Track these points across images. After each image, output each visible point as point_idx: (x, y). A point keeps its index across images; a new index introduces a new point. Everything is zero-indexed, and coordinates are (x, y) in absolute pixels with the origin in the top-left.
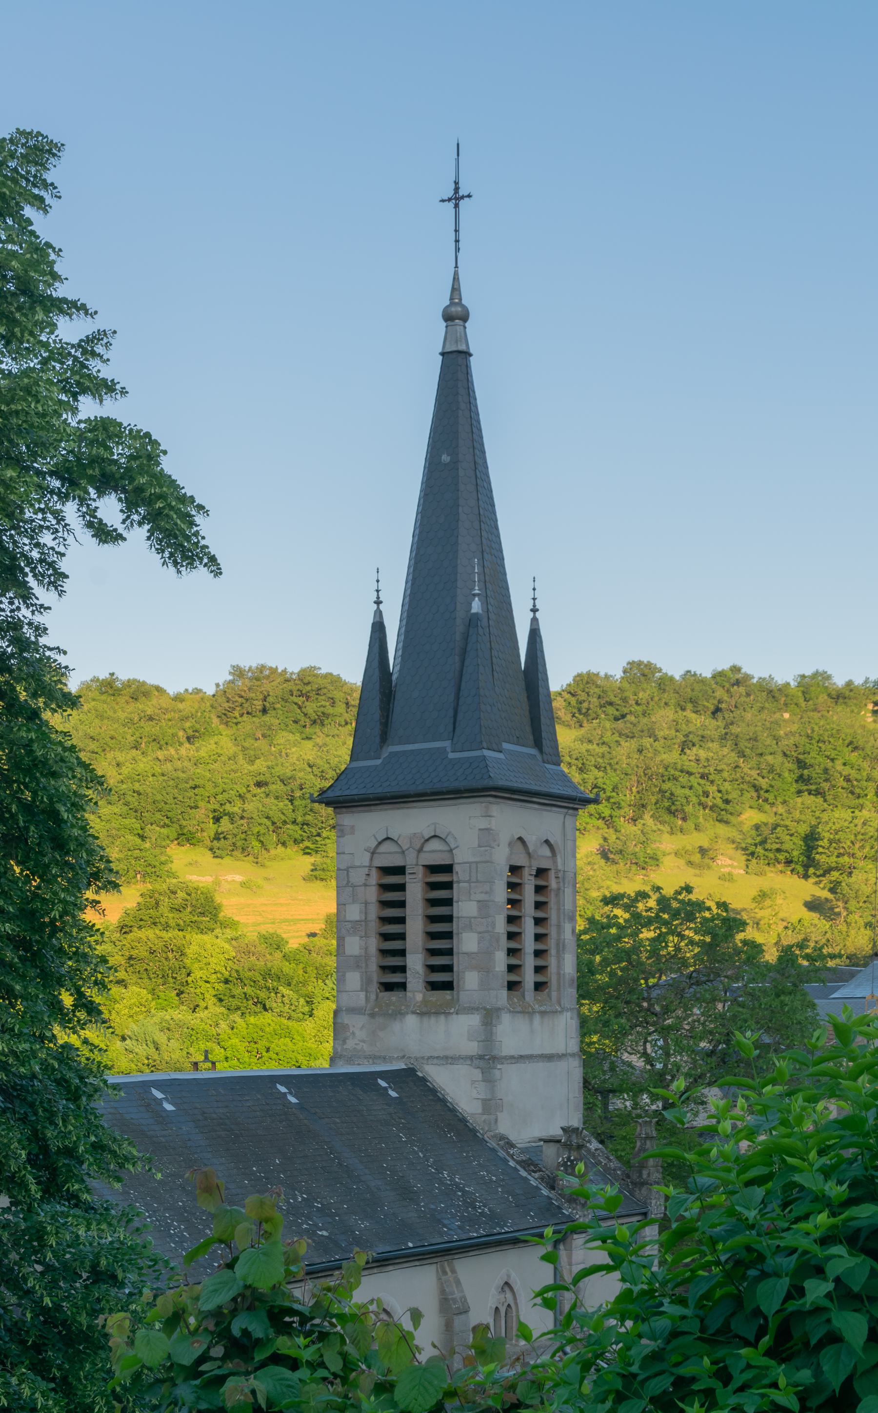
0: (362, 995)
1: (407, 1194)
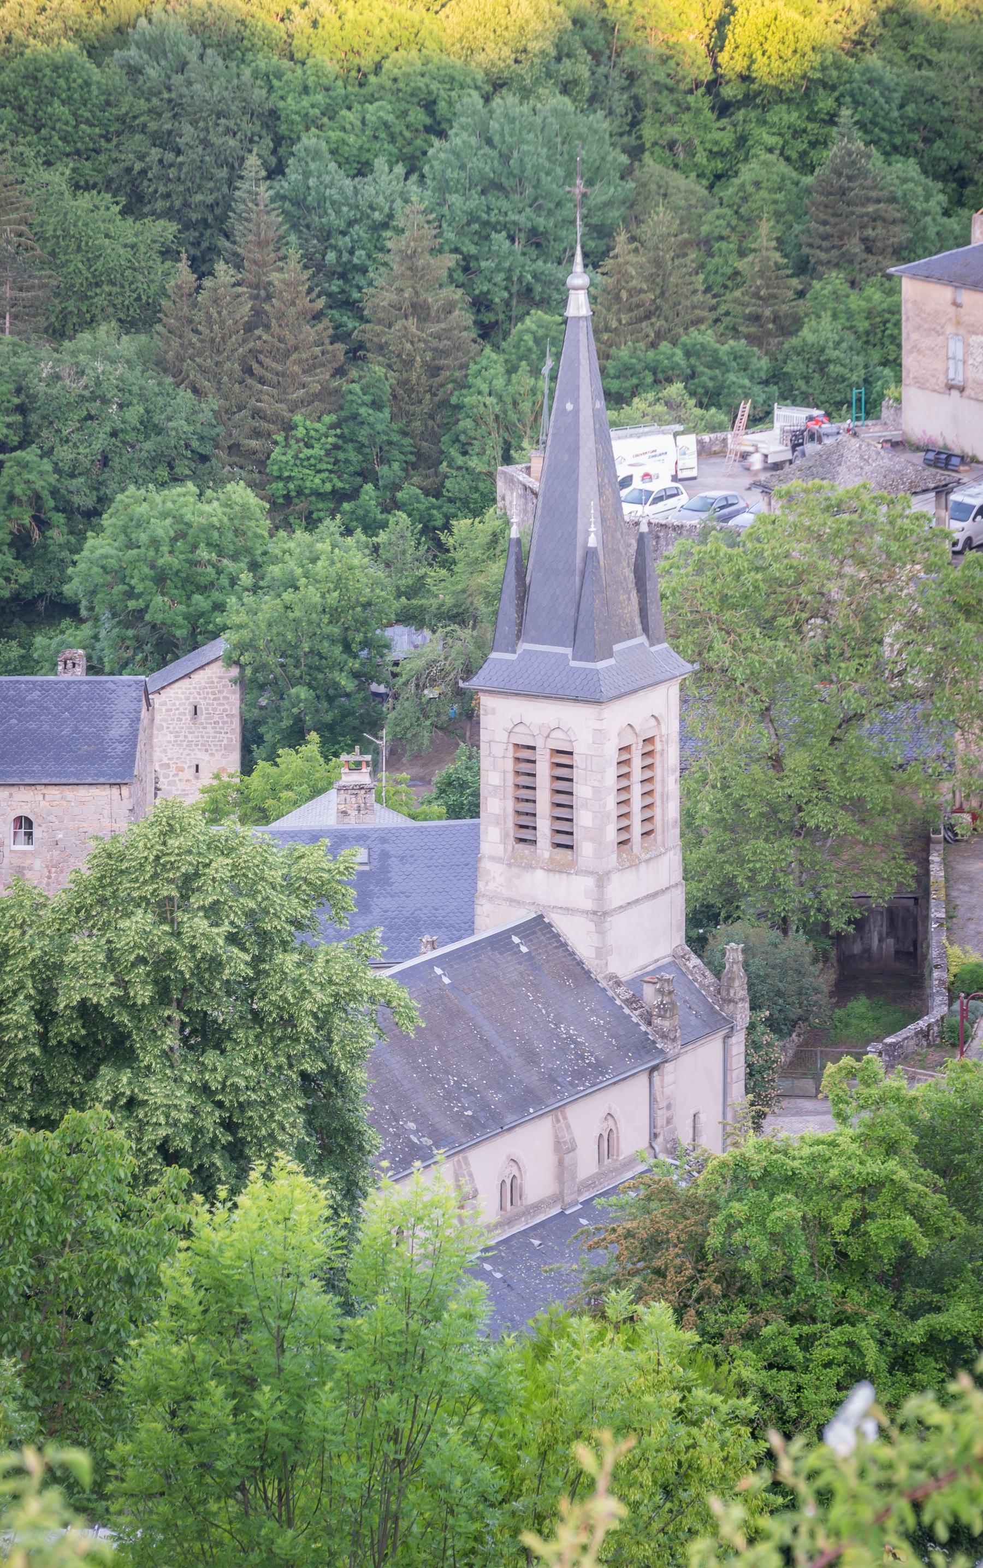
0: (501, 847)
1: (531, 1057)
